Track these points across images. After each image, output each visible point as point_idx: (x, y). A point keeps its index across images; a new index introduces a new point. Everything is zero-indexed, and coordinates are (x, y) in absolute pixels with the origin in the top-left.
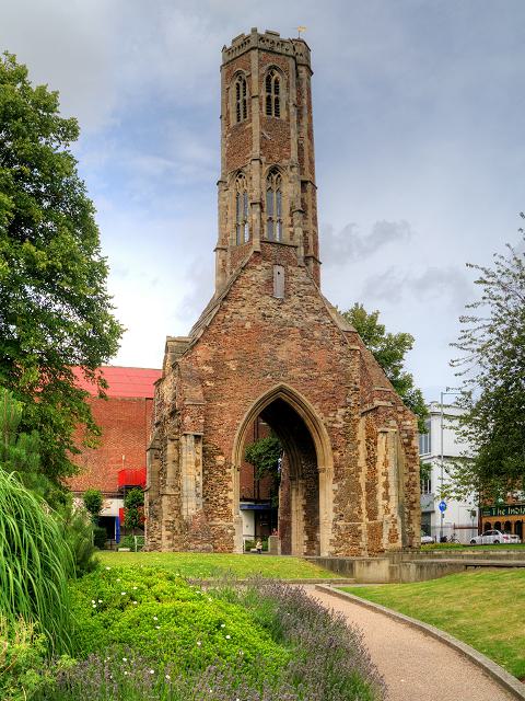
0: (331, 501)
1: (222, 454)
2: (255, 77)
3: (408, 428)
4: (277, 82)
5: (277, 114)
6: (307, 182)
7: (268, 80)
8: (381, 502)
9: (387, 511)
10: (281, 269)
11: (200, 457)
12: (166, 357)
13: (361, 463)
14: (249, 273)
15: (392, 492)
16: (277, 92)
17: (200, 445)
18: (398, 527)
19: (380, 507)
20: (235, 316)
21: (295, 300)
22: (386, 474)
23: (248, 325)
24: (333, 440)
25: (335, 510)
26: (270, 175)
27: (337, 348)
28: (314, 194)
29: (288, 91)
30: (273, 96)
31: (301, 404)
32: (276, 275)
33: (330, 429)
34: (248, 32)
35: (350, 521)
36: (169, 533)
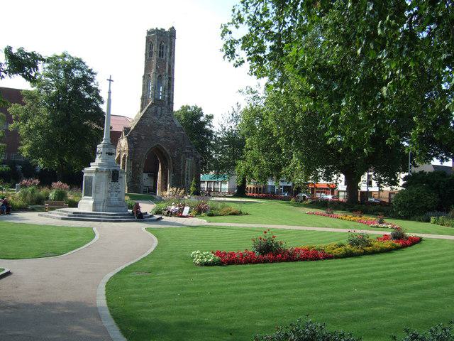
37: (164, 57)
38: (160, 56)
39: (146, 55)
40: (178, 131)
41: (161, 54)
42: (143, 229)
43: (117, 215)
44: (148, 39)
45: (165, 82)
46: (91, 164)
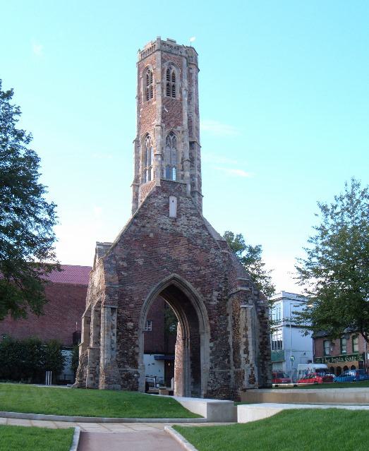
0: (208, 354)
1: (131, 321)
3: (261, 305)
4: (173, 74)
5: (174, 96)
6: (194, 142)
7: (168, 71)
8: (243, 356)
9: (247, 361)
11: (115, 323)
12: (96, 256)
13: (229, 329)
15: (251, 348)
17: (115, 315)
18: (256, 373)
19: (242, 359)
20: (142, 229)
22: (246, 336)
23: (151, 235)
24: (209, 313)
25: (211, 361)
26: (168, 136)
27: (213, 251)
28: (201, 200)
29: (181, 80)
30: (172, 83)
32: (171, 201)
33: (207, 305)
35: (222, 369)
36: (92, 375)
38: (168, 94)
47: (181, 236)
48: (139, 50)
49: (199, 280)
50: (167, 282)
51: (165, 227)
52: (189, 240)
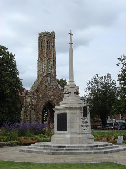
2: (45, 41)
10: (50, 78)
14: (44, 79)
16: (49, 44)
21: (52, 84)
31: (53, 102)
34: (44, 32)
37: (50, 49)
38: (48, 48)
39: (39, 47)
40: (61, 92)
41: (48, 46)
42: (18, 151)
43: (104, 149)
44: (40, 38)
45: (51, 63)
46: (60, 103)
47: (51, 88)
48: (39, 33)
49: (56, 101)
50: (48, 101)
51: (47, 86)
52: (53, 90)
